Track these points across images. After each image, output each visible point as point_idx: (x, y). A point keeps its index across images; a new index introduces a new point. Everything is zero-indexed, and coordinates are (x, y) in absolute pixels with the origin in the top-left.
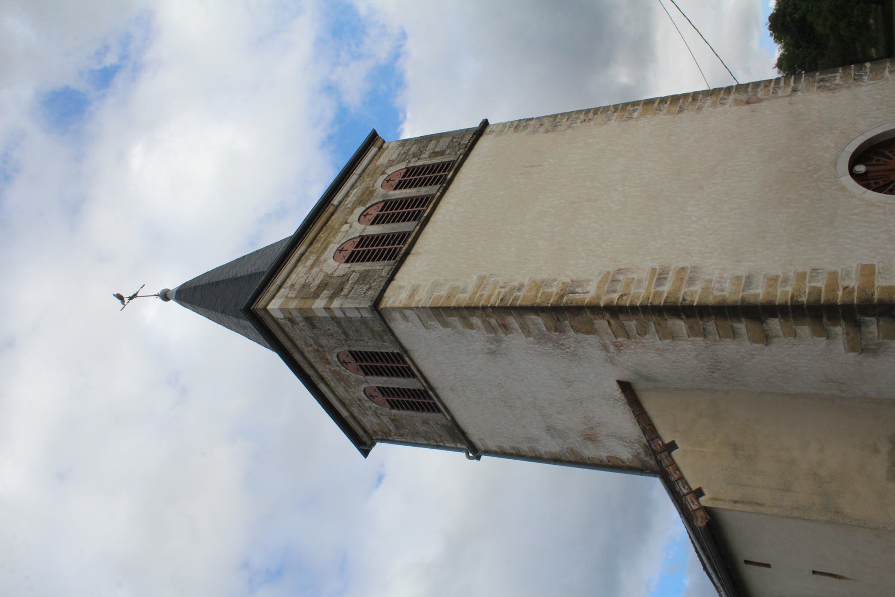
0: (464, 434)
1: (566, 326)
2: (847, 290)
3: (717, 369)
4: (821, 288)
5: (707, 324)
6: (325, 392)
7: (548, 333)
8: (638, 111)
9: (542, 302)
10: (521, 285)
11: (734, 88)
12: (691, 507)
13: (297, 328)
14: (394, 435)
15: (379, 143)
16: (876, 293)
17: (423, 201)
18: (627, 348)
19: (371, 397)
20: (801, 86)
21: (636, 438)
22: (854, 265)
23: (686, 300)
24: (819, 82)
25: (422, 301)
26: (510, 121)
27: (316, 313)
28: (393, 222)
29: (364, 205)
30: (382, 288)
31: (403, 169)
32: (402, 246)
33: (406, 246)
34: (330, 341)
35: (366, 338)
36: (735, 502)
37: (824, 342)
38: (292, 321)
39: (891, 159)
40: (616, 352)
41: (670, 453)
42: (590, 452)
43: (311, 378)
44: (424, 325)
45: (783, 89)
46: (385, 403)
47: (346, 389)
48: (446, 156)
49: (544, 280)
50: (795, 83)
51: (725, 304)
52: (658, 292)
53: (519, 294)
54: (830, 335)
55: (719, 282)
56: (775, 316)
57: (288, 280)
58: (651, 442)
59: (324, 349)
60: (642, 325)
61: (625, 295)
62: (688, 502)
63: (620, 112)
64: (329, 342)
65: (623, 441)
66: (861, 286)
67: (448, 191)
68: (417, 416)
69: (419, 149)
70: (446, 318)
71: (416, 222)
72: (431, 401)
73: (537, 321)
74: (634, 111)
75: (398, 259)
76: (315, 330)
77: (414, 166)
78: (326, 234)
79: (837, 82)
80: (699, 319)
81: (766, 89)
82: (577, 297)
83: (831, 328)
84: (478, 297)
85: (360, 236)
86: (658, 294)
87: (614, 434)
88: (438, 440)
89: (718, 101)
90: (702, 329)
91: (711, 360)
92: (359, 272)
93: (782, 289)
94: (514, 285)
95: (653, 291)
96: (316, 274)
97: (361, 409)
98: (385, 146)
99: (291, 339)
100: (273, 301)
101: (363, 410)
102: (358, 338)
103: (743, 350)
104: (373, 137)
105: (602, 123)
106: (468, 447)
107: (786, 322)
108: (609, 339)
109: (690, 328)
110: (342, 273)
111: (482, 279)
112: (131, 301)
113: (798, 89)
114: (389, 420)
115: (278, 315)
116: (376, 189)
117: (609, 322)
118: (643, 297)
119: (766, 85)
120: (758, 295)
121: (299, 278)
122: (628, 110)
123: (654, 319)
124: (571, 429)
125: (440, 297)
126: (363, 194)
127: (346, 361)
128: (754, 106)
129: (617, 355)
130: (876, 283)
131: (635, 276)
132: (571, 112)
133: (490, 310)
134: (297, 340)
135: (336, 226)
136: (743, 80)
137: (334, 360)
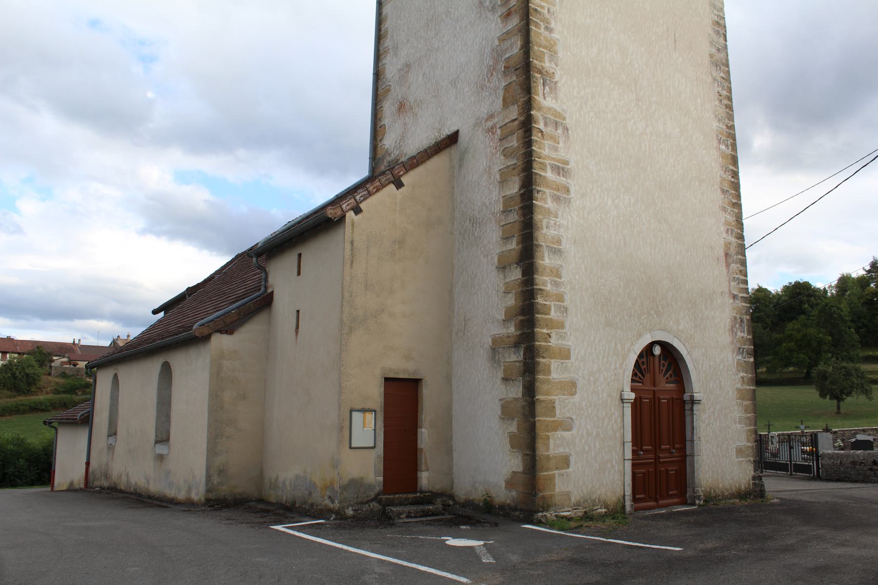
1: (511, 77)
3: (473, 224)
4: (550, 315)
5: (516, 213)
7: (503, 60)
8: (726, 150)
9: (534, 52)
10: (552, 30)
11: (742, 243)
12: (344, 204)
18: (490, 139)
21: (405, 152)
22: (570, 342)
24: (740, 318)
36: (352, 243)
37: (500, 318)
39: (664, 376)
41: (393, 183)
42: (388, 107)
45: (737, 286)
49: (557, 54)
50: (742, 297)
52: (546, 166)
53: (542, 29)
56: (524, 274)
58: (401, 165)
61: (543, 135)
63: (726, 132)
65: (401, 139)
73: (515, 47)
74: (727, 146)
79: (739, 333)
80: (519, 206)
83: (513, 323)
86: (544, 167)
89: (730, 227)
90: (510, 209)
94: (551, 23)
95: (547, 162)
103: (492, 247)
105: (717, 114)
108: (499, 121)
109: (511, 198)
117: (516, 119)
118: (541, 153)
119: (743, 271)
120: (543, 260)
122: (728, 139)
124: (409, 88)
128: (723, 259)
129: (483, 129)
130: (553, 360)
131: (561, 145)
136: (748, 253)
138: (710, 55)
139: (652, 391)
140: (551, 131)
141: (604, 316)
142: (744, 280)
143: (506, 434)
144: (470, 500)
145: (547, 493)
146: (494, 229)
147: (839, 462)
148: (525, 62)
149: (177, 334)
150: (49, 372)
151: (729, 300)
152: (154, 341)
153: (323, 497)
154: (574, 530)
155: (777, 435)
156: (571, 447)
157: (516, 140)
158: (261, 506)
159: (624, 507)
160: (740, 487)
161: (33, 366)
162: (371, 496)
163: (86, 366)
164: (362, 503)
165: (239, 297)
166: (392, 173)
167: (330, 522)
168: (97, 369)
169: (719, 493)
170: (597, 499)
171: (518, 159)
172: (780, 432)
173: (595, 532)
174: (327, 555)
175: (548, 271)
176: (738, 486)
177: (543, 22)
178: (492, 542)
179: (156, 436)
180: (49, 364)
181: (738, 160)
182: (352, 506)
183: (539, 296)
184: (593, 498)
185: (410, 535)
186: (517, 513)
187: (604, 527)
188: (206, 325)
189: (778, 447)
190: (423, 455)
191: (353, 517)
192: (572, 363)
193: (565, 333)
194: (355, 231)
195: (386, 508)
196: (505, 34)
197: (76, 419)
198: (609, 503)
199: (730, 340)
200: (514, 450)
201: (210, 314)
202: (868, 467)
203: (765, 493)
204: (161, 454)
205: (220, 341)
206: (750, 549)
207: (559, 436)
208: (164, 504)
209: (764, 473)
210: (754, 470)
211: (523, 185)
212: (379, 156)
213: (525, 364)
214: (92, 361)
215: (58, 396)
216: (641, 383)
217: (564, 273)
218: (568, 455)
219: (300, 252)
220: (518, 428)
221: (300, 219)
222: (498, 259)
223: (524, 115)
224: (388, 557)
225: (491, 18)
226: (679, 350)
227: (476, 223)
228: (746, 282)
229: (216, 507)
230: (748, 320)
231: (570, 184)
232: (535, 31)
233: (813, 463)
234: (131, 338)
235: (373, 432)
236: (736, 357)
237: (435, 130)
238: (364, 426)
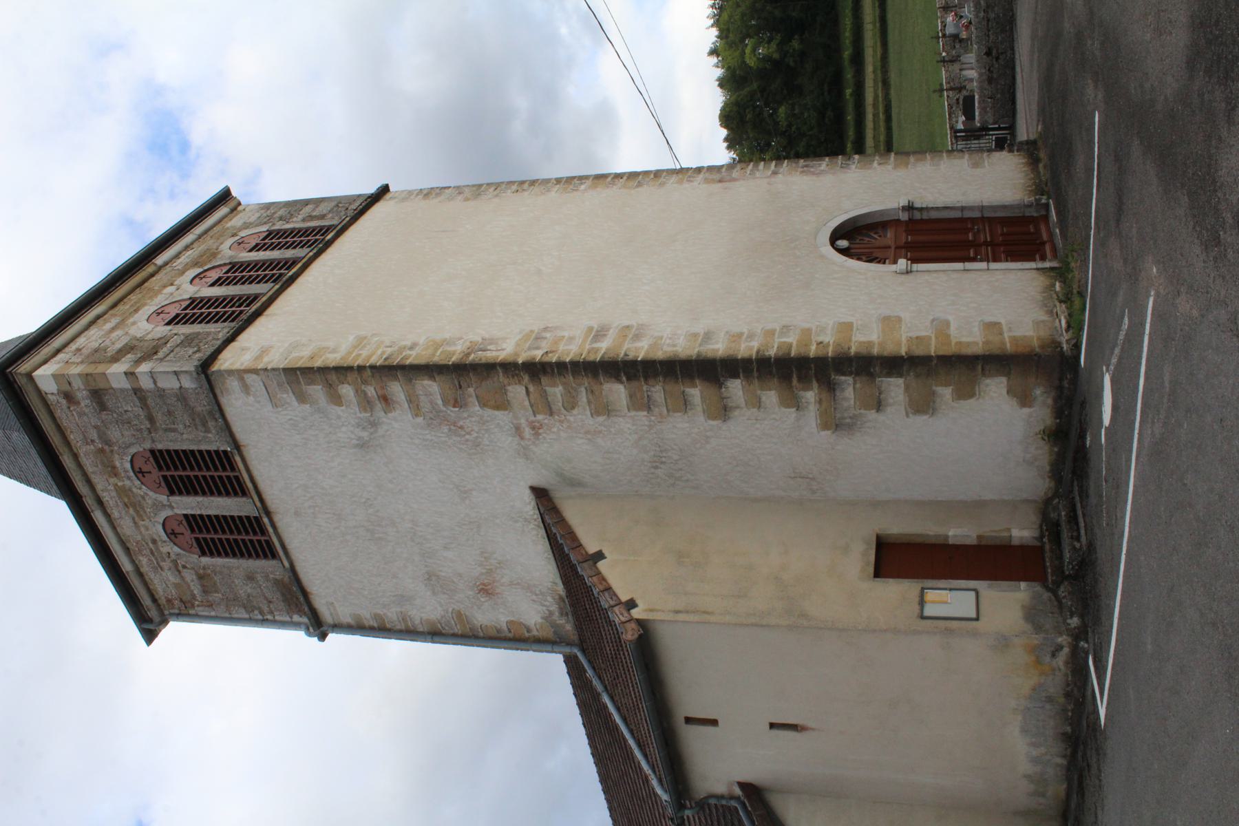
0: (305, 594)
1: (470, 396)
5: (653, 389)
6: (101, 526)
7: (445, 409)
8: (586, 184)
13: (74, 410)
14: (198, 606)
15: (232, 204)
18: (548, 432)
27: (111, 382)
31: (264, 232)
34: (126, 433)
36: (677, 612)
37: (794, 415)
38: (69, 397)
40: (532, 438)
41: (596, 563)
42: (486, 616)
43: (84, 499)
47: (135, 523)
51: (677, 359)
52: (593, 348)
54: (800, 404)
55: (670, 338)
56: (736, 376)
59: (112, 448)
61: (551, 352)
63: (564, 184)
64: (122, 435)
65: (531, 592)
72: (262, 538)
73: (431, 388)
77: (279, 230)
78: (140, 296)
79: (822, 168)
80: (643, 383)
82: (488, 355)
83: (802, 393)
85: (190, 298)
87: (520, 581)
88: (266, 609)
93: (747, 344)
95: (587, 347)
97: (153, 558)
98: (240, 208)
99: (62, 430)
101: (156, 559)
102: (169, 426)
104: (224, 197)
107: (750, 385)
114: (194, 577)
117: (527, 388)
121: (90, 342)
123: (586, 384)
124: (460, 575)
125: (301, 357)
128: (727, 185)
129: (534, 443)
131: (566, 334)
132: (501, 183)
133: (369, 370)
134: (71, 432)
139: (897, 250)
140: (547, 343)
144: (1052, 471)
145: (1036, 343)
147: (989, 100)
153: (1053, 670)
157: (553, 388)
159: (1052, 269)
160: (1023, 163)
171: (580, 385)
182: (1065, 621)
184: (1041, 299)
190: (988, 534)
191: (1082, 616)
192: (857, 320)
196: (411, 405)
198: (1048, 283)
200: (977, 393)
202: (995, 62)
213: (857, 373)
218: (982, 323)
219: (683, 720)
222: (713, 420)
225: (385, 427)
233: (992, 135)
238: (946, 603)
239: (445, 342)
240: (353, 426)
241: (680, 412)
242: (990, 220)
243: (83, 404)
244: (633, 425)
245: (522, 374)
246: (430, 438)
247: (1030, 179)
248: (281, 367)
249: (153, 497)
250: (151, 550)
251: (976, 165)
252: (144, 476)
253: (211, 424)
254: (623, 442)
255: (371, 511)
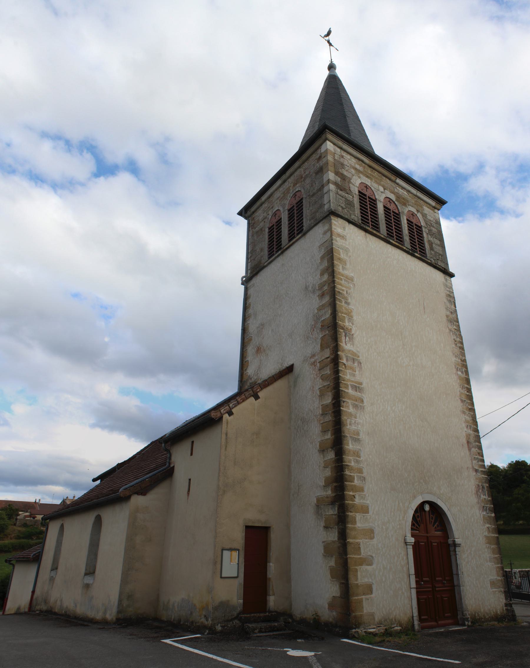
2: (353, 497)
3: (303, 422)
4: (354, 482)
5: (330, 415)
8: (462, 375)
9: (339, 317)
11: (478, 434)
12: (222, 409)
14: (252, 231)
15: (438, 206)
16: (352, 514)
17: (400, 239)
18: (313, 369)
19: (275, 214)
20: (479, 474)
22: (368, 502)
23: (343, 403)
24: (482, 485)
25: (336, 243)
26: (454, 292)
28: (386, 220)
29: (396, 200)
30: (344, 216)
32: (371, 227)
33: (371, 230)
34: (308, 186)
35: (311, 208)
36: (226, 434)
38: (320, 158)
39: (433, 526)
40: (311, 362)
41: (253, 396)
42: (250, 350)
43: (284, 175)
44: (321, 245)
46: (272, 223)
47: (279, 198)
48: (429, 251)
50: (481, 471)
52: (348, 386)
54: (326, 487)
55: (355, 422)
56: (336, 455)
57: (346, 153)
58: (258, 385)
60: (328, 377)
61: (345, 367)
62: (225, 407)
63: (461, 364)
64: (307, 184)
65: (258, 369)
66: (355, 505)
67: (407, 254)
68: (265, 244)
69: (434, 233)
70: (326, 258)
71: (386, 235)
72: (275, 252)
73: (327, 314)
74: (462, 372)
75: (362, 225)
76: (315, 175)
77: (422, 231)
78: (377, 176)
79: (482, 496)
81: (477, 454)
83: (330, 488)
84: (340, 278)
85: (376, 199)
86: (347, 386)
87: (261, 364)
88: (252, 258)
89: (469, 424)
90: (326, 413)
91: (308, 418)
92: (353, 200)
96: (351, 172)
98: (436, 211)
100: (332, 144)
102: (311, 203)
103: (315, 437)
105: (454, 352)
106: (248, 277)
109: (327, 406)
110: (352, 189)
111: (352, 279)
112: (327, 42)
113: (477, 472)
114: (261, 227)
115: (323, 149)
116: (407, 208)
117: (328, 357)
118: (344, 377)
119: (480, 453)
120: (348, 446)
121: (347, 161)
122: (463, 368)
123: (331, 384)
124: (263, 338)
126: (404, 199)
127: (296, 197)
131: (357, 373)
133: (333, 285)
134: (308, 163)
135: (382, 183)
137: (296, 189)
138: (446, 316)
140: (350, 364)
141: (390, 483)
142: (482, 459)
143: (328, 568)
145: (358, 614)
146: (317, 426)
148: (333, 323)
149: (108, 495)
150: (15, 523)
151: (473, 473)
152: (92, 500)
154: (379, 644)
155: (519, 572)
156: (373, 578)
157: (329, 369)
158: (156, 624)
159: (413, 625)
160: (497, 612)
161: (4, 519)
162: (234, 615)
163: (42, 518)
164: (228, 621)
165: (151, 470)
166: (252, 390)
167: (204, 636)
168: (49, 521)
169: (482, 616)
170: (393, 619)
172: (520, 569)
173: (394, 646)
174: (201, 664)
175: (352, 453)
176: (495, 611)
177: (344, 299)
178: (320, 653)
179: (86, 570)
180: (15, 518)
181: (470, 381)
183: (346, 470)
184: (390, 618)
185: (261, 647)
186: (337, 629)
187: (401, 642)
188: (128, 489)
189: (520, 581)
191: (221, 632)
192: (370, 516)
193: (364, 495)
194: (228, 426)
195: (245, 625)
196: (321, 307)
197: (30, 558)
199: (476, 501)
200: (333, 580)
201: (132, 481)
203: (516, 618)
204: (88, 584)
205: (137, 500)
206: (512, 664)
207: (364, 569)
208: (86, 623)
209: (513, 601)
210: (505, 598)
211: (334, 397)
212: (244, 379)
213: (339, 516)
214: (47, 515)
215: (19, 540)
216: (417, 530)
217: (362, 454)
218: (371, 583)
219: (192, 440)
220: (336, 563)
221: (194, 419)
222: (319, 445)
223: (334, 354)
224: (246, 665)
226: (441, 506)
227: (305, 422)
228: (483, 461)
229: (124, 625)
230: (488, 487)
231: (364, 397)
232: (339, 304)
234: (76, 498)
235: (237, 565)
236: (482, 513)
237: (279, 364)
238: (231, 561)
239: (351, 318)
240: (313, 283)
241: (322, 429)
242: (454, 590)
243: (317, 165)
244: (316, 408)
245: (334, 354)
246: (310, 317)
247: (484, 616)
248: (334, 246)
249: (287, 203)
250: (270, 207)
251: (493, 584)
252: (294, 197)
253: (312, 221)
254: (310, 404)
255: (284, 296)
